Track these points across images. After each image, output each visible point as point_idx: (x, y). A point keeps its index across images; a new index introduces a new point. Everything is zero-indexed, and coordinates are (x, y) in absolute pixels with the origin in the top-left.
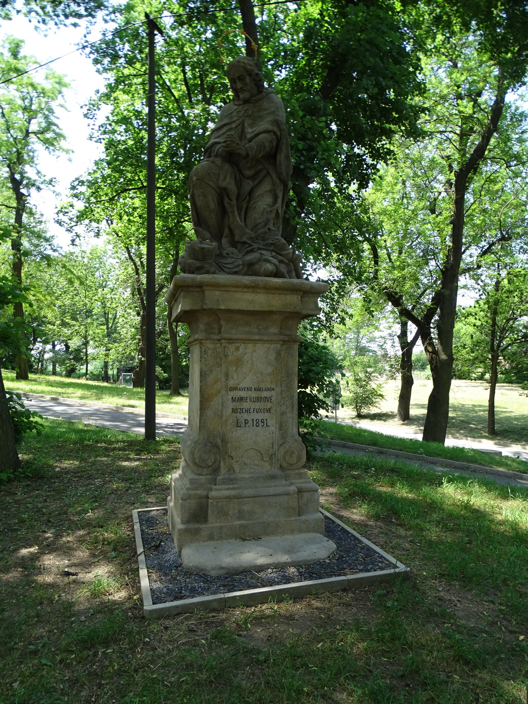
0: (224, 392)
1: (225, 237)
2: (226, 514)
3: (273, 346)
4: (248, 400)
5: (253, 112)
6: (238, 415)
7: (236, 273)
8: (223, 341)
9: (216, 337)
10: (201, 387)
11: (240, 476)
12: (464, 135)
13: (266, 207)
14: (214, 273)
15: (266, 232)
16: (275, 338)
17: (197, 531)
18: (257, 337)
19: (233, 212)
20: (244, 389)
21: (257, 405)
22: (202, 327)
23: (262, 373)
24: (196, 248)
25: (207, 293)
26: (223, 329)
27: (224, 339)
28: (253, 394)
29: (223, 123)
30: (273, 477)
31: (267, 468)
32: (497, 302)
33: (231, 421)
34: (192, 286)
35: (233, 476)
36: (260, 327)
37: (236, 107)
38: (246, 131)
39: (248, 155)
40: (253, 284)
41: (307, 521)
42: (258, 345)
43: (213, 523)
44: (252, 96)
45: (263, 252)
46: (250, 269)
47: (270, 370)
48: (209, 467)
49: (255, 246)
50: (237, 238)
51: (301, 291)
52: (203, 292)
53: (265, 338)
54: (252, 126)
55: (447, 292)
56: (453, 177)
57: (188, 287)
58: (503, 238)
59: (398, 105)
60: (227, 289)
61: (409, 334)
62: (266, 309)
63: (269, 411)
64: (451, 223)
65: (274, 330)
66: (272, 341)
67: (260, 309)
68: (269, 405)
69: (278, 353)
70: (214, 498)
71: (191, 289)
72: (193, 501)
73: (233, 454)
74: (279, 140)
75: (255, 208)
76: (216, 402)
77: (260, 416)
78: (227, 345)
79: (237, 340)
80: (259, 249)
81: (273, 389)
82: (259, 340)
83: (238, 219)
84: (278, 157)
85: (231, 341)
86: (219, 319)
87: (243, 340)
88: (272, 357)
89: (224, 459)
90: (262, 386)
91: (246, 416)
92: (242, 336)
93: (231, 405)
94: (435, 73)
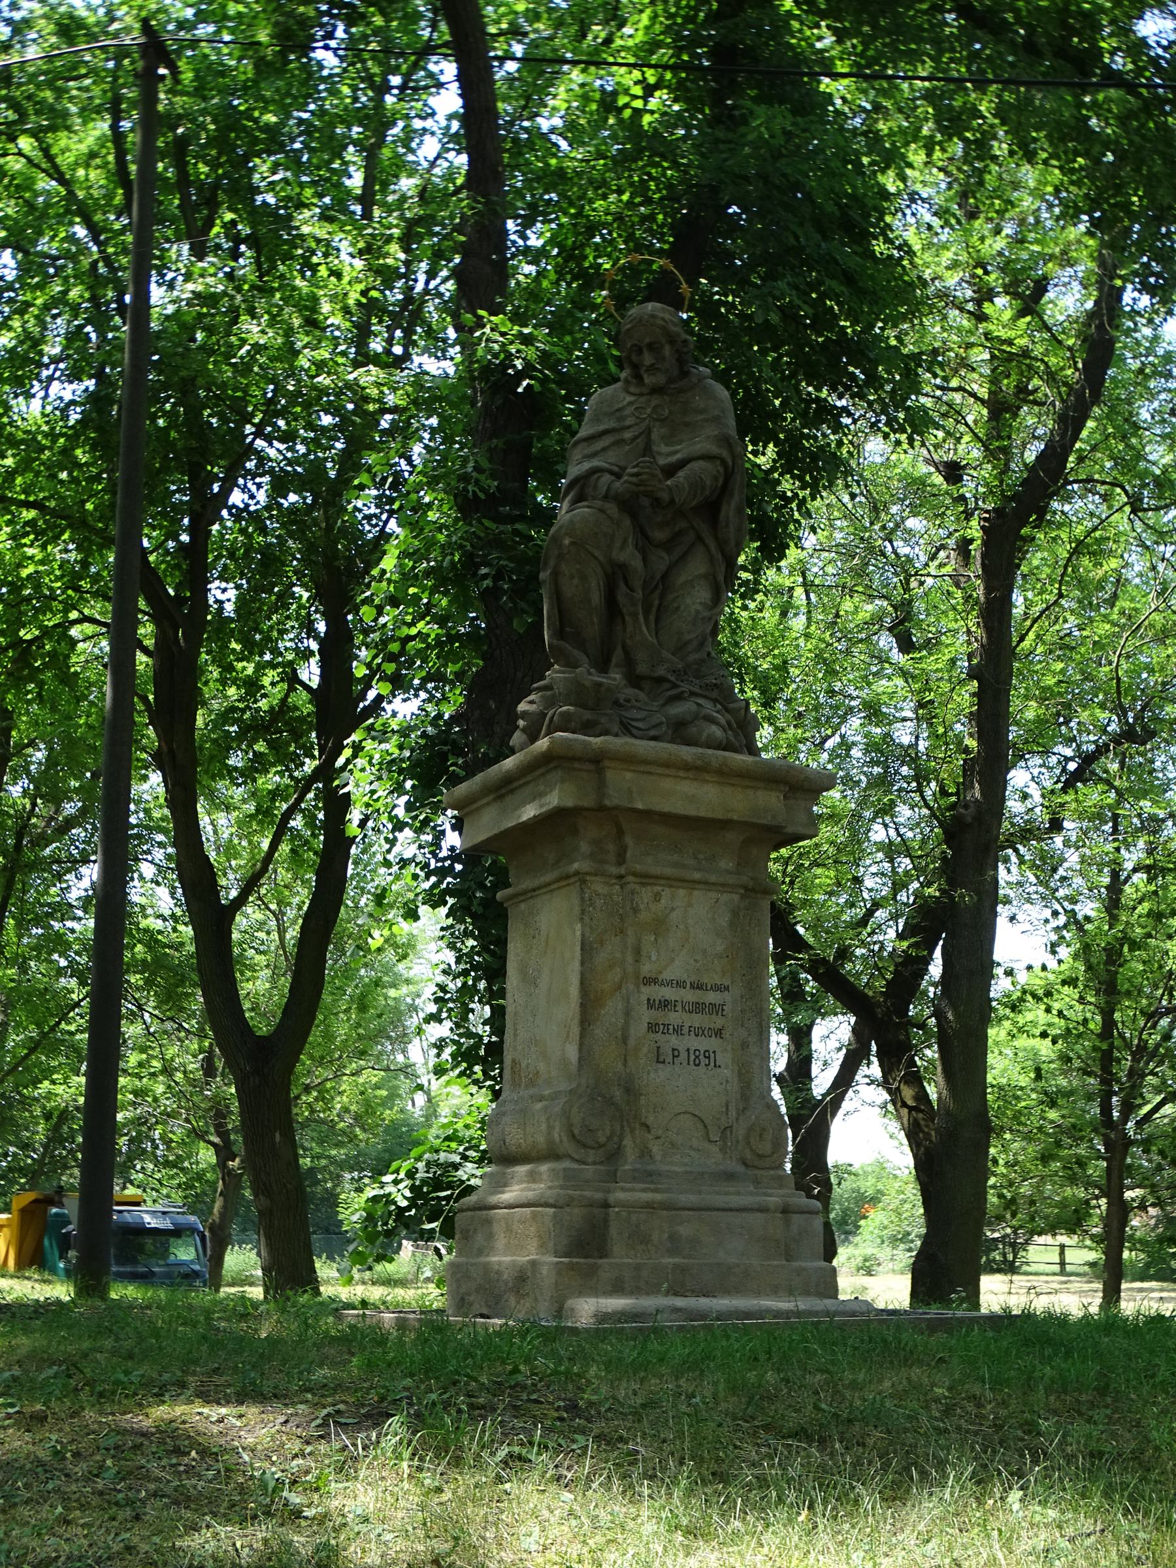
0: (631, 987)
1: (617, 666)
2: (645, 1240)
3: (725, 897)
4: (679, 1008)
5: (671, 412)
6: (659, 1036)
7: (654, 738)
8: (630, 878)
9: (614, 870)
10: (582, 974)
11: (664, 1168)
12: (1000, 409)
13: (700, 608)
14: (616, 735)
15: (703, 661)
16: (732, 880)
17: (593, 1271)
18: (697, 876)
19: (634, 615)
20: (670, 983)
21: (697, 1020)
22: (584, 847)
23: (705, 951)
24: (587, 683)
25: (609, 774)
26: (628, 855)
27: (635, 874)
28: (689, 996)
29: (602, 428)
30: (730, 1176)
31: (715, 1158)
32: (1113, 955)
33: (645, 1050)
34: (579, 759)
35: (650, 1167)
36: (701, 856)
37: (629, 399)
38: (655, 448)
39: (672, 501)
40: (699, 763)
41: (804, 1269)
42: (696, 893)
43: (621, 1256)
44: (671, 381)
45: (701, 701)
46: (680, 731)
47: (720, 947)
48: (601, 1146)
49: (685, 687)
50: (642, 669)
51: (786, 783)
52: (600, 772)
53: (713, 878)
54: (668, 440)
55: (965, 896)
56: (974, 530)
57: (574, 759)
58: (1128, 735)
59: (865, 351)
60: (648, 768)
61: (815, 1069)
62: (720, 815)
63: (719, 1033)
64: (972, 675)
65: (726, 864)
66: (723, 887)
67: (710, 815)
68: (719, 1022)
69: (735, 913)
70: (619, 1204)
71: (577, 765)
72: (576, 1211)
73: (650, 1120)
74: (728, 475)
75: (678, 608)
76: (611, 1011)
77: (701, 1044)
78: (637, 887)
79: (657, 877)
80: (692, 694)
81: (727, 989)
82: (699, 883)
83: (644, 628)
84: (724, 509)
85: (646, 878)
86: (620, 833)
87: (668, 879)
88: (724, 920)
89: (632, 1131)
90: (706, 980)
91: (674, 1040)
92: (668, 871)
93: (646, 1016)
94: (922, 227)
